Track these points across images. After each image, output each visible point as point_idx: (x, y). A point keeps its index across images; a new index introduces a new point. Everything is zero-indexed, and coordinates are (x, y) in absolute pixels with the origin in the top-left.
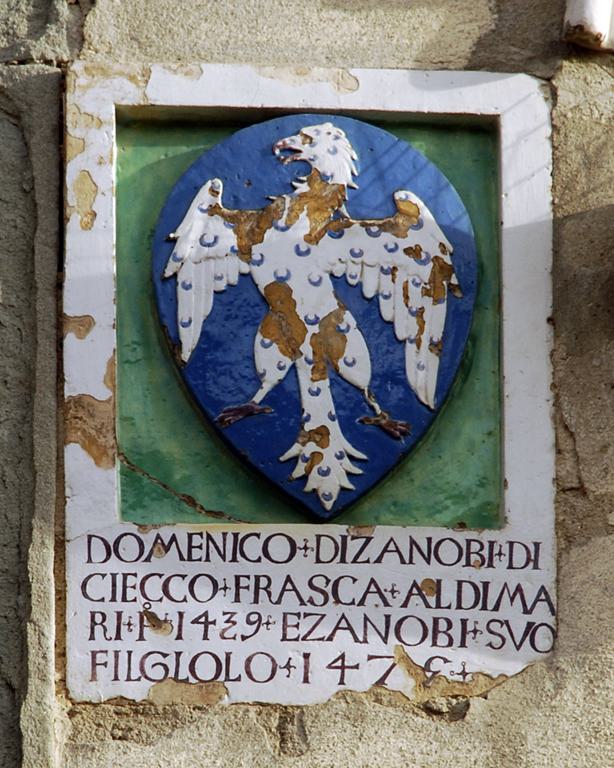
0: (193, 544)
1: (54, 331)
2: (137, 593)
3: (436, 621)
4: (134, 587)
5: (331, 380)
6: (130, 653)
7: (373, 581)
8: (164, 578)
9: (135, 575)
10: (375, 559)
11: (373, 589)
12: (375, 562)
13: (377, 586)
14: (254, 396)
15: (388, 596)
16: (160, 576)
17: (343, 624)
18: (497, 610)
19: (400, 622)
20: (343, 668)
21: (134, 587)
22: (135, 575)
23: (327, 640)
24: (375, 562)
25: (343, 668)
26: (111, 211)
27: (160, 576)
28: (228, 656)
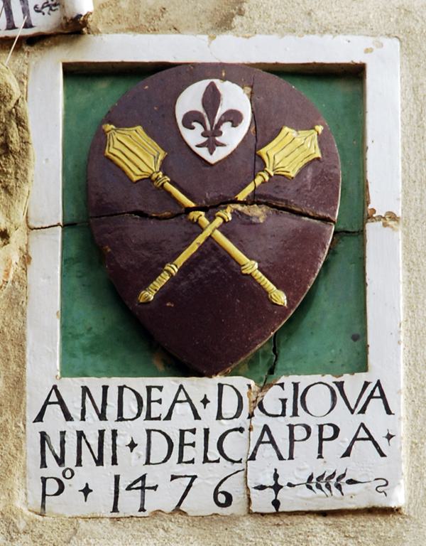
0: (324, 437)
1: (66, 439)
3: (295, 414)
5: (208, 140)
15: (199, 407)
17: (182, 397)
18: (170, 419)
20: (143, 488)
23: (165, 419)
25: (143, 488)
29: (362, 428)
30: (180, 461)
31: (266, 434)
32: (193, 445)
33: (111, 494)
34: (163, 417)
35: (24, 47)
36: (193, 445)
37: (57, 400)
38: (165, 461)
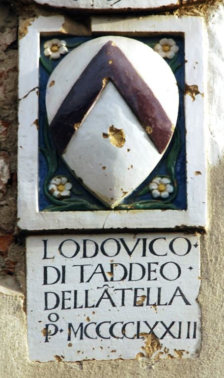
7: (178, 288)
8: (97, 324)
9: (157, 263)
10: (87, 280)
12: (87, 282)
13: (180, 291)
14: (16, 219)
16: (96, 323)
19: (57, 306)
22: (157, 263)
23: (169, 304)
24: (87, 282)
26: (93, 108)
27: (96, 323)
29: (99, 266)
30: (149, 279)
31: (178, 291)
32: (69, 299)
33: (60, 214)
34: (168, 304)
35: (197, 234)
36: (69, 299)
37: (180, 294)
38: (142, 278)
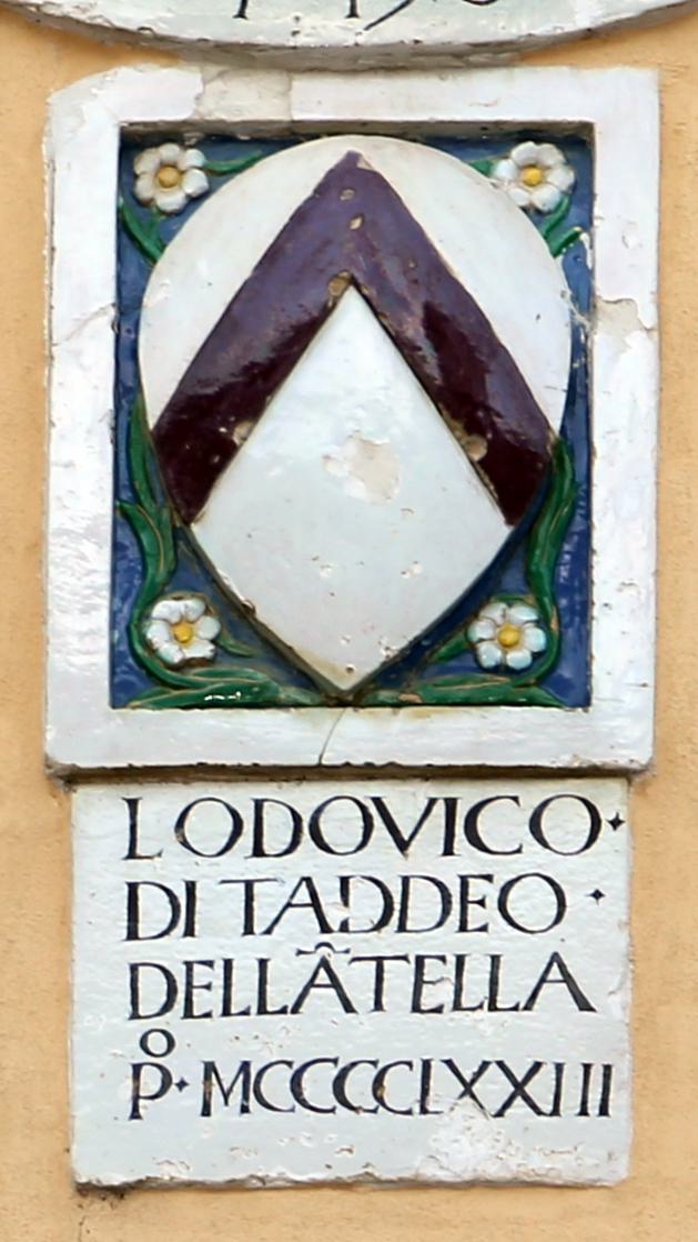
2: (491, 913)
4: (481, 903)
6: (584, 1112)
9: (489, 878)
11: (323, 977)
16: (289, 1064)
21: (481, 903)
22: (489, 878)
27: (289, 1064)
28: (191, 888)
